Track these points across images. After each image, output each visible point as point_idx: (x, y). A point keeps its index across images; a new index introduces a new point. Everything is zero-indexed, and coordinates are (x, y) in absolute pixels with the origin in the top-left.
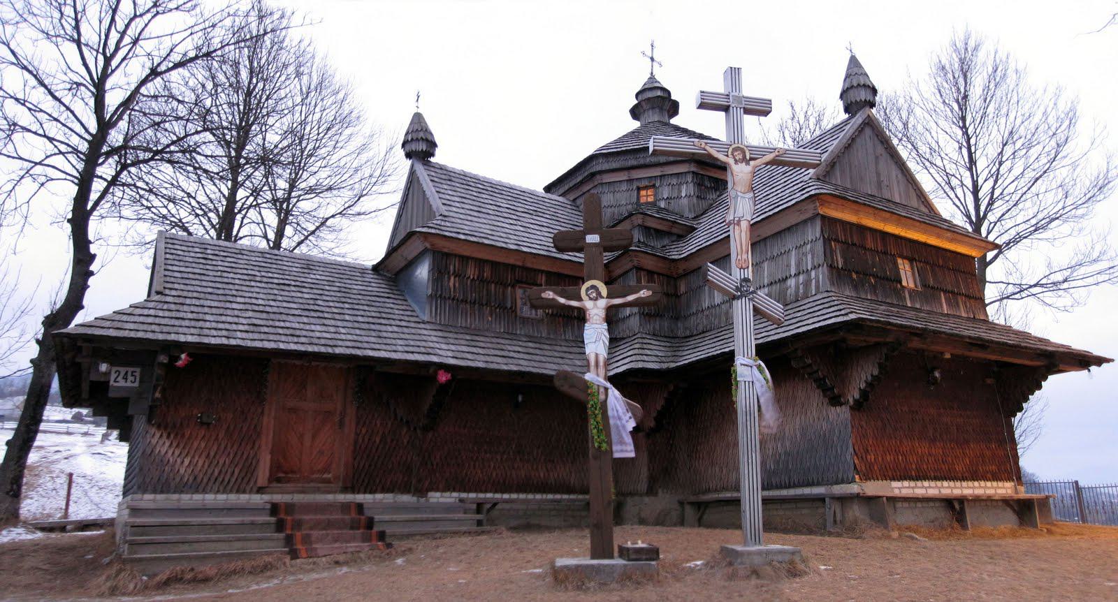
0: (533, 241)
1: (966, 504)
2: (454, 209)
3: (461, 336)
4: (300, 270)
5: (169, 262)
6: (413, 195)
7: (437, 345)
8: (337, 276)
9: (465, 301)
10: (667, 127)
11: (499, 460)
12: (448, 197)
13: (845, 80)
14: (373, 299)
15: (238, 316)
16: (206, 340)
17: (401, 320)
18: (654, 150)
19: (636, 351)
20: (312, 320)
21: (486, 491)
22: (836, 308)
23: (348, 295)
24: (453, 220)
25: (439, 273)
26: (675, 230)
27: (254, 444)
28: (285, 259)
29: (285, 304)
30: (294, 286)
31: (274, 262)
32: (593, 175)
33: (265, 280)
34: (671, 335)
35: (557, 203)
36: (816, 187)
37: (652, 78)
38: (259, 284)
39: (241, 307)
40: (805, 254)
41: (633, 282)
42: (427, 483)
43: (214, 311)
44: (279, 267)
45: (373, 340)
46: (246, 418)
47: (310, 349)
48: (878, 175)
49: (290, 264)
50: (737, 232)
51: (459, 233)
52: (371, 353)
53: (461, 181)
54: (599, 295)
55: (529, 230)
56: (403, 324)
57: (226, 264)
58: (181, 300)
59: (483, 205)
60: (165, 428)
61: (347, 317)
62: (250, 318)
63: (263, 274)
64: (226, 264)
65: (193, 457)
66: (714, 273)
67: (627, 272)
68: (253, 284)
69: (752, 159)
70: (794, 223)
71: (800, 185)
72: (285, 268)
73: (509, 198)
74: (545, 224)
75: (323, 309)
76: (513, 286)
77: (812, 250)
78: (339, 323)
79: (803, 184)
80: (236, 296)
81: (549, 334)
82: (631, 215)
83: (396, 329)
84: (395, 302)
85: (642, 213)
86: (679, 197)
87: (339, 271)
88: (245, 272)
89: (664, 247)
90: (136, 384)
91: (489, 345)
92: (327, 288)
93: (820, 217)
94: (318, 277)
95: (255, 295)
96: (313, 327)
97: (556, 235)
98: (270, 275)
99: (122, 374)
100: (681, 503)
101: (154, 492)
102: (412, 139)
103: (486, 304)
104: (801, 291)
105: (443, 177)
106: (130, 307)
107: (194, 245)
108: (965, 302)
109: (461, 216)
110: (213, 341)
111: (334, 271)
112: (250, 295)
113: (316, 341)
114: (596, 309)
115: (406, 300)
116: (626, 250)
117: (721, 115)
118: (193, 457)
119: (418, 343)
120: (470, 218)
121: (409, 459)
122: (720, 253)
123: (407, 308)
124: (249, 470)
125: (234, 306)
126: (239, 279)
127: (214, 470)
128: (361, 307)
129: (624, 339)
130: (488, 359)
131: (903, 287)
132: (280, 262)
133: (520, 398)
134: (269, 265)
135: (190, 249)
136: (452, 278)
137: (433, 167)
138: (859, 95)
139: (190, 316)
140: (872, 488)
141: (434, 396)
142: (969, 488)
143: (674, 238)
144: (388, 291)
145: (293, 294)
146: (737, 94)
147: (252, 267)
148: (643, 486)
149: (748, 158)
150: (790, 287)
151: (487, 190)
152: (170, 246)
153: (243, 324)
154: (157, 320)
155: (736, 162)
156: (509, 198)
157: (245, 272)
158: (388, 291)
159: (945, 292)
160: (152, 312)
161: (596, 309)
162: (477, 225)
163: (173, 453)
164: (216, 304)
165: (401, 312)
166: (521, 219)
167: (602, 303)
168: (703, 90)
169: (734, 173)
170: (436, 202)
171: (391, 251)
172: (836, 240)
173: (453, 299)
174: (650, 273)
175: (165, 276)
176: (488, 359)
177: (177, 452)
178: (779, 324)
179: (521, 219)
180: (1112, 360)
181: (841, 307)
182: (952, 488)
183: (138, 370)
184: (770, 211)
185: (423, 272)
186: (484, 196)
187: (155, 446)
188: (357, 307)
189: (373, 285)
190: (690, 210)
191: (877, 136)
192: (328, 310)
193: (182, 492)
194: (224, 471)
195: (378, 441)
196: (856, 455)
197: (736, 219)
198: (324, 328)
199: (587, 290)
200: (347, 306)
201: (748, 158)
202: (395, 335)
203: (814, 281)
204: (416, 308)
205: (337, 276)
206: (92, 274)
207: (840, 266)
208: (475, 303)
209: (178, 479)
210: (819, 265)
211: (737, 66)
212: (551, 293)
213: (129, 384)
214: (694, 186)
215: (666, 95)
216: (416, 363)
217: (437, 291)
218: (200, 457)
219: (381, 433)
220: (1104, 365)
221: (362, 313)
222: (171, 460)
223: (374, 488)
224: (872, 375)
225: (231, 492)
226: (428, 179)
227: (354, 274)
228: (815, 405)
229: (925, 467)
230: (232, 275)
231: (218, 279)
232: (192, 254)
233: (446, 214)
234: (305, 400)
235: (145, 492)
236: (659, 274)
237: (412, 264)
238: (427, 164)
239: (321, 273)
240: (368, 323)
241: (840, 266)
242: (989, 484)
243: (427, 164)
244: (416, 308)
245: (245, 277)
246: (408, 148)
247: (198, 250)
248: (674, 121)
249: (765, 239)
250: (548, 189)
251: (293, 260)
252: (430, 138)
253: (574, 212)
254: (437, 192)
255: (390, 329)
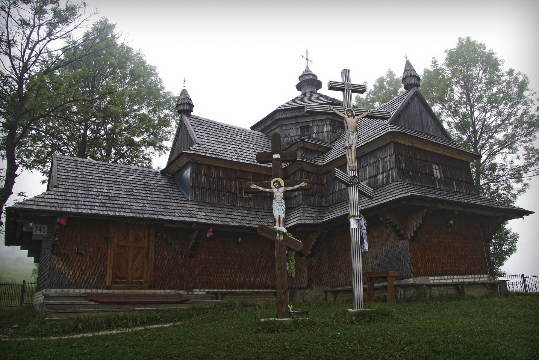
0: (245, 156)
1: (465, 287)
2: (204, 140)
3: (208, 208)
4: (124, 174)
5: (60, 170)
6: (182, 133)
7: (196, 213)
8: (143, 176)
9: (210, 189)
10: (315, 95)
11: (229, 272)
12: (200, 134)
13: (404, 73)
14: (162, 188)
15: (95, 198)
16: (80, 211)
17: (176, 200)
18: (307, 111)
19: (301, 214)
20: (132, 200)
21: (223, 289)
22: (401, 190)
23: (149, 187)
24: (203, 146)
25: (195, 174)
26: (320, 150)
27: (104, 264)
28: (116, 168)
29: (117, 192)
30: (122, 182)
31: (111, 169)
32: (277, 121)
33: (107, 179)
34: (319, 205)
35: (258, 136)
36: (391, 128)
37: (307, 69)
38: (104, 182)
39: (96, 193)
40: (386, 162)
41: (298, 179)
42: (192, 284)
43: (83, 196)
44: (113, 172)
45: (162, 210)
46: (100, 251)
47: (131, 215)
48: (422, 121)
49: (119, 170)
50: (350, 152)
51: (206, 153)
52: (162, 217)
53: (207, 125)
54: (280, 186)
55: (243, 151)
56: (178, 201)
57: (87, 171)
58: (67, 190)
59: (219, 138)
60: (60, 256)
61: (149, 198)
62: (100, 199)
63: (106, 176)
64: (87, 171)
65: (74, 270)
66: (339, 173)
67: (295, 173)
68: (101, 181)
69: (356, 115)
70: (380, 146)
71: (383, 127)
72: (116, 173)
73: (232, 133)
74: (252, 147)
75: (137, 194)
76: (235, 181)
77: (390, 160)
78: (145, 202)
79: (384, 126)
80: (93, 188)
81: (254, 205)
82: (297, 142)
83: (174, 204)
84: (173, 190)
85: (303, 141)
86: (323, 132)
87: (144, 174)
88: (97, 175)
89: (315, 158)
90: (45, 233)
91: (223, 212)
92: (138, 183)
93: (393, 143)
94: (133, 177)
95: (102, 187)
96: (132, 204)
97: (257, 155)
98: (109, 176)
99: (38, 229)
100: (325, 292)
101: (56, 288)
102: (181, 103)
103: (221, 191)
104: (385, 181)
105: (198, 123)
106: (42, 194)
107: (71, 161)
108: (465, 185)
109: (207, 144)
110: (84, 211)
111: (141, 174)
112: (100, 187)
113: (134, 211)
114: (279, 193)
115: (179, 189)
116: (294, 161)
117: (341, 93)
118: (74, 270)
119: (186, 212)
120: (212, 145)
121: (183, 272)
122: (341, 161)
123: (180, 193)
124: (102, 277)
125: (93, 193)
126: (94, 179)
127: (84, 277)
128: (156, 193)
129: (294, 208)
130: (223, 219)
131: (435, 178)
132: (114, 170)
133: (240, 240)
134: (109, 171)
135: (69, 163)
136: (203, 177)
137: (192, 118)
138: (411, 80)
139: (71, 198)
140: (419, 280)
141: (195, 239)
142: (466, 278)
143: (320, 154)
144: (169, 184)
145: (121, 186)
146: (348, 83)
147: (100, 173)
148: (305, 284)
149: (354, 115)
150: (380, 179)
151: (221, 129)
152: (59, 162)
153: (98, 203)
154: (56, 201)
155: (349, 117)
156: (232, 133)
157: (97, 175)
158: (169, 184)
159: (456, 180)
160: (53, 197)
161: (279, 193)
162: (216, 148)
163: (64, 268)
164: (84, 192)
165: (177, 196)
166: (239, 144)
167: (282, 190)
168: (331, 81)
169: (348, 122)
170: (194, 136)
171: (170, 163)
172: (402, 155)
173: (204, 188)
174: (308, 172)
175: (58, 178)
176: (223, 219)
177: (66, 268)
178: (371, 198)
179: (239, 144)
180: (534, 212)
181: (403, 189)
182: (458, 279)
183: (46, 226)
184: (368, 140)
185: (188, 173)
186: (219, 132)
187: (56, 265)
188: (153, 193)
189: (162, 181)
190: (328, 139)
191: (421, 101)
192: (139, 194)
193: (69, 288)
194: (89, 278)
195: (166, 262)
196: (412, 264)
197: (349, 146)
198: (138, 204)
199: (274, 183)
200: (149, 192)
201: (354, 115)
202: (174, 208)
203: (391, 176)
204: (185, 193)
205: (143, 176)
206: (17, 176)
207: (404, 168)
208: (215, 189)
209: (67, 282)
210: (393, 168)
211: (348, 69)
212: (255, 185)
213: (42, 233)
214: (330, 126)
215: (315, 78)
216: (185, 222)
217: (195, 184)
218: (77, 270)
219: (167, 259)
220: (530, 215)
221: (156, 196)
222: (63, 272)
223: (165, 287)
224: (419, 223)
225: (93, 288)
226: (189, 124)
227: (151, 175)
228: (392, 240)
229: (446, 269)
230: (90, 177)
231: (84, 179)
232: (71, 166)
233: (200, 143)
234: (129, 242)
235: (51, 288)
236: (312, 173)
237: (183, 169)
238: (189, 116)
239: (135, 175)
240: (160, 201)
241: (404, 168)
242: (476, 276)
243: (189, 116)
244: (185, 193)
245: (97, 178)
246: (179, 108)
247: (73, 164)
248: (319, 91)
249: (366, 154)
250: (253, 128)
251: (120, 168)
252: (190, 102)
253: (267, 140)
254: (194, 131)
255: (171, 204)
